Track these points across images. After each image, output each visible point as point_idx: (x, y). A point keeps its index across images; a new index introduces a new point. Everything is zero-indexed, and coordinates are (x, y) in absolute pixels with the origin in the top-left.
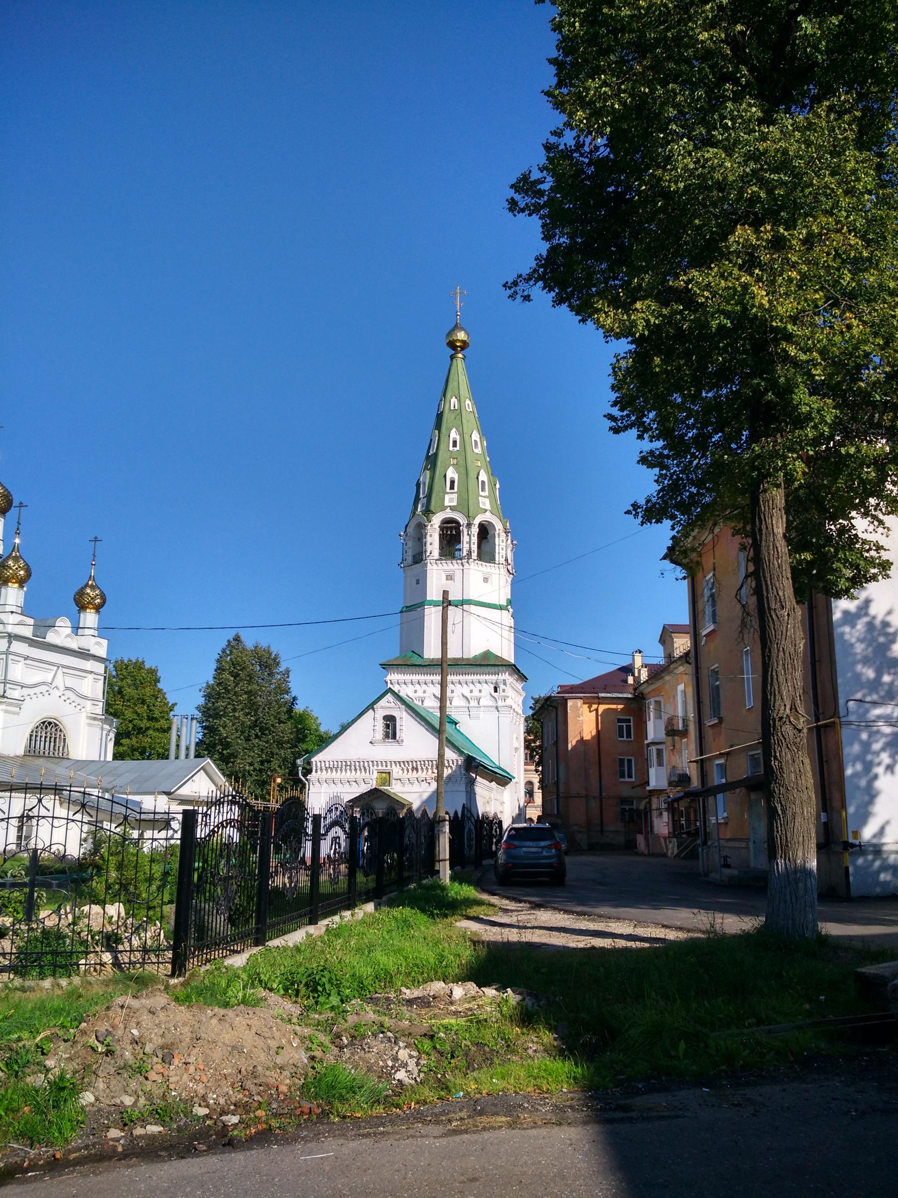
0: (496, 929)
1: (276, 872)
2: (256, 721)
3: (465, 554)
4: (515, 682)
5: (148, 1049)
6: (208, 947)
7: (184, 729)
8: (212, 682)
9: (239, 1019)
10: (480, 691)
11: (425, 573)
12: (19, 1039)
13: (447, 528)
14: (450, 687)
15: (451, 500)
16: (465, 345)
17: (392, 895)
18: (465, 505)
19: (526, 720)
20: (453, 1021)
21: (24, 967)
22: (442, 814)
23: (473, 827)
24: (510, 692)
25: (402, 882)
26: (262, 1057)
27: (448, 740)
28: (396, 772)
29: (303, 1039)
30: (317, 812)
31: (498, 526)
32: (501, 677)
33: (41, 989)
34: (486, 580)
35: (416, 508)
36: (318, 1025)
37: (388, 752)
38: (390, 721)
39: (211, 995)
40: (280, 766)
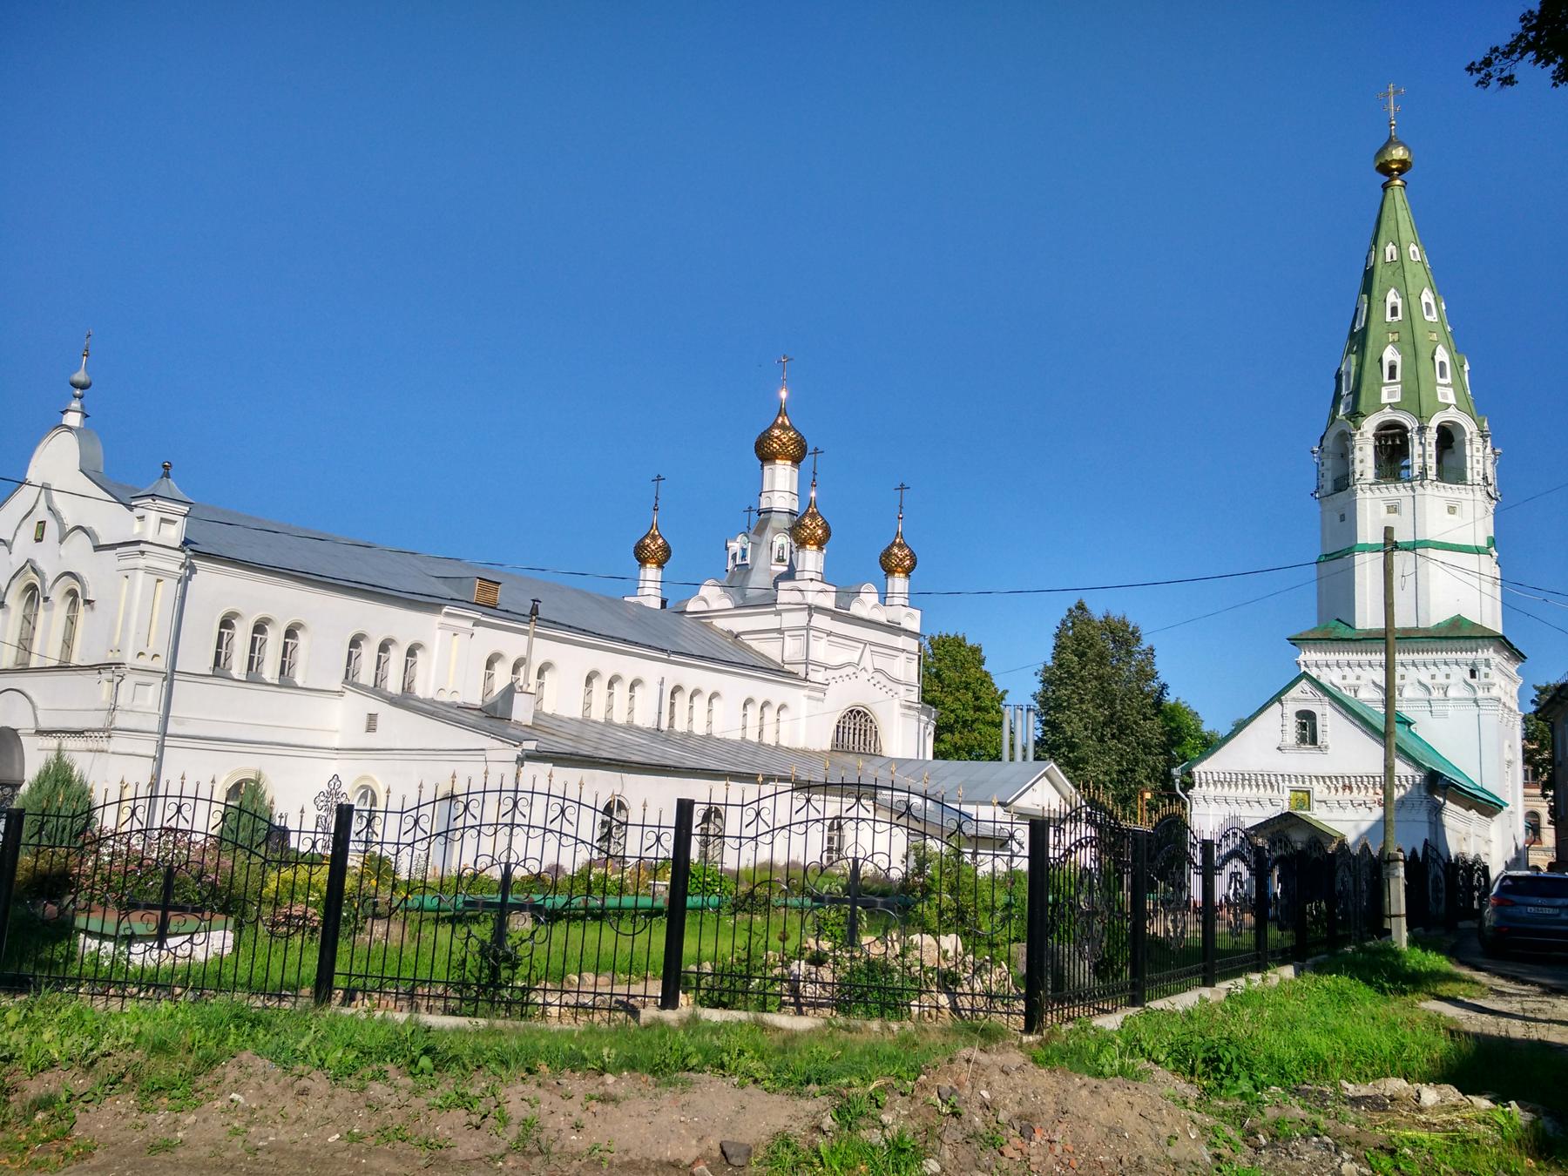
0: (1484, 1017)
1: (1156, 911)
2: (1112, 715)
3: (1416, 472)
4: (1505, 663)
5: (1002, 1117)
6: (1069, 1000)
7: (1019, 723)
8: (1050, 664)
9: (1118, 1095)
10: (1448, 676)
11: (1353, 505)
12: (850, 1086)
13: (1386, 436)
14: (1399, 670)
15: (1391, 395)
16: (1404, 166)
17: (1320, 958)
18: (1415, 401)
19: (1525, 720)
20: (1425, 1135)
21: (848, 1003)
22: (1392, 850)
23: (1440, 873)
24: (1496, 677)
25: (1333, 943)
26: (1149, 1146)
27: (1399, 748)
28: (1319, 791)
29: (1203, 1130)
30: (1207, 837)
31: (1469, 427)
32: (1482, 655)
33: (870, 1031)
34: (1452, 510)
35: (1336, 411)
36: (1223, 1114)
37: (1305, 762)
38: (1307, 720)
39: (1078, 1059)
40: (1148, 778)
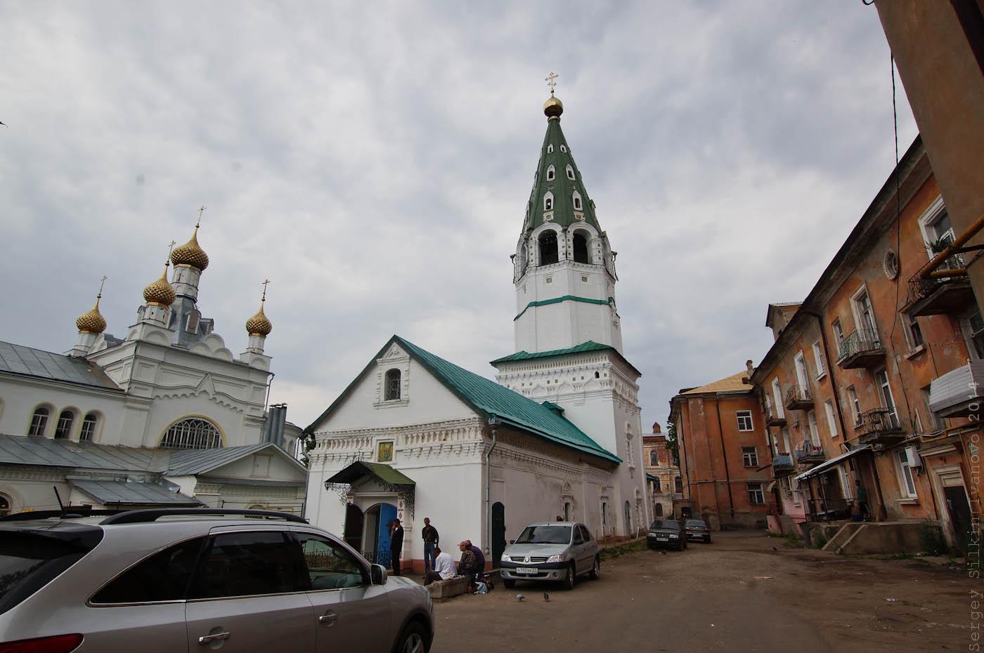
28: (399, 444)
37: (394, 416)
